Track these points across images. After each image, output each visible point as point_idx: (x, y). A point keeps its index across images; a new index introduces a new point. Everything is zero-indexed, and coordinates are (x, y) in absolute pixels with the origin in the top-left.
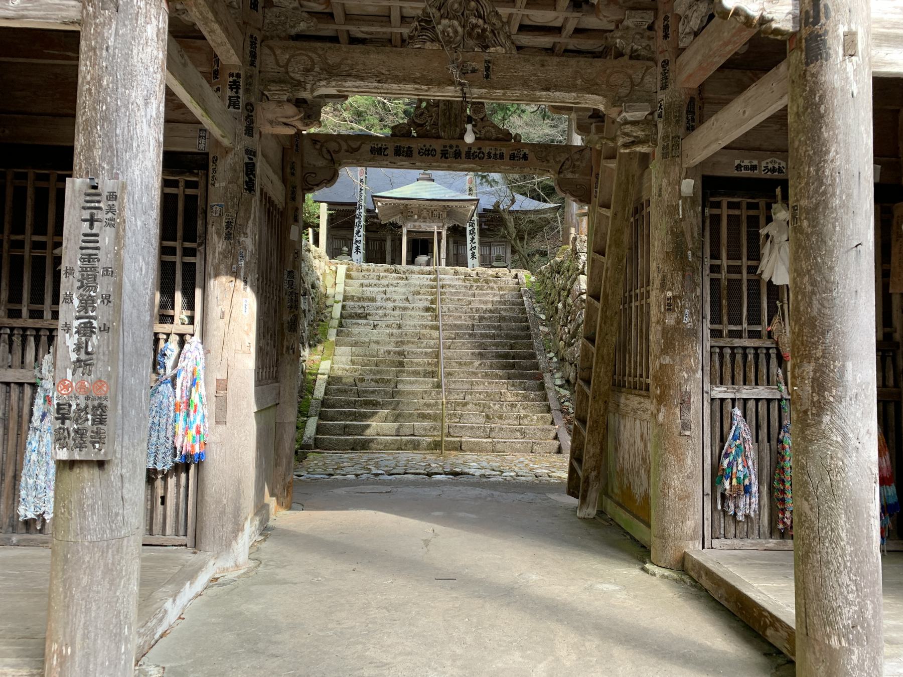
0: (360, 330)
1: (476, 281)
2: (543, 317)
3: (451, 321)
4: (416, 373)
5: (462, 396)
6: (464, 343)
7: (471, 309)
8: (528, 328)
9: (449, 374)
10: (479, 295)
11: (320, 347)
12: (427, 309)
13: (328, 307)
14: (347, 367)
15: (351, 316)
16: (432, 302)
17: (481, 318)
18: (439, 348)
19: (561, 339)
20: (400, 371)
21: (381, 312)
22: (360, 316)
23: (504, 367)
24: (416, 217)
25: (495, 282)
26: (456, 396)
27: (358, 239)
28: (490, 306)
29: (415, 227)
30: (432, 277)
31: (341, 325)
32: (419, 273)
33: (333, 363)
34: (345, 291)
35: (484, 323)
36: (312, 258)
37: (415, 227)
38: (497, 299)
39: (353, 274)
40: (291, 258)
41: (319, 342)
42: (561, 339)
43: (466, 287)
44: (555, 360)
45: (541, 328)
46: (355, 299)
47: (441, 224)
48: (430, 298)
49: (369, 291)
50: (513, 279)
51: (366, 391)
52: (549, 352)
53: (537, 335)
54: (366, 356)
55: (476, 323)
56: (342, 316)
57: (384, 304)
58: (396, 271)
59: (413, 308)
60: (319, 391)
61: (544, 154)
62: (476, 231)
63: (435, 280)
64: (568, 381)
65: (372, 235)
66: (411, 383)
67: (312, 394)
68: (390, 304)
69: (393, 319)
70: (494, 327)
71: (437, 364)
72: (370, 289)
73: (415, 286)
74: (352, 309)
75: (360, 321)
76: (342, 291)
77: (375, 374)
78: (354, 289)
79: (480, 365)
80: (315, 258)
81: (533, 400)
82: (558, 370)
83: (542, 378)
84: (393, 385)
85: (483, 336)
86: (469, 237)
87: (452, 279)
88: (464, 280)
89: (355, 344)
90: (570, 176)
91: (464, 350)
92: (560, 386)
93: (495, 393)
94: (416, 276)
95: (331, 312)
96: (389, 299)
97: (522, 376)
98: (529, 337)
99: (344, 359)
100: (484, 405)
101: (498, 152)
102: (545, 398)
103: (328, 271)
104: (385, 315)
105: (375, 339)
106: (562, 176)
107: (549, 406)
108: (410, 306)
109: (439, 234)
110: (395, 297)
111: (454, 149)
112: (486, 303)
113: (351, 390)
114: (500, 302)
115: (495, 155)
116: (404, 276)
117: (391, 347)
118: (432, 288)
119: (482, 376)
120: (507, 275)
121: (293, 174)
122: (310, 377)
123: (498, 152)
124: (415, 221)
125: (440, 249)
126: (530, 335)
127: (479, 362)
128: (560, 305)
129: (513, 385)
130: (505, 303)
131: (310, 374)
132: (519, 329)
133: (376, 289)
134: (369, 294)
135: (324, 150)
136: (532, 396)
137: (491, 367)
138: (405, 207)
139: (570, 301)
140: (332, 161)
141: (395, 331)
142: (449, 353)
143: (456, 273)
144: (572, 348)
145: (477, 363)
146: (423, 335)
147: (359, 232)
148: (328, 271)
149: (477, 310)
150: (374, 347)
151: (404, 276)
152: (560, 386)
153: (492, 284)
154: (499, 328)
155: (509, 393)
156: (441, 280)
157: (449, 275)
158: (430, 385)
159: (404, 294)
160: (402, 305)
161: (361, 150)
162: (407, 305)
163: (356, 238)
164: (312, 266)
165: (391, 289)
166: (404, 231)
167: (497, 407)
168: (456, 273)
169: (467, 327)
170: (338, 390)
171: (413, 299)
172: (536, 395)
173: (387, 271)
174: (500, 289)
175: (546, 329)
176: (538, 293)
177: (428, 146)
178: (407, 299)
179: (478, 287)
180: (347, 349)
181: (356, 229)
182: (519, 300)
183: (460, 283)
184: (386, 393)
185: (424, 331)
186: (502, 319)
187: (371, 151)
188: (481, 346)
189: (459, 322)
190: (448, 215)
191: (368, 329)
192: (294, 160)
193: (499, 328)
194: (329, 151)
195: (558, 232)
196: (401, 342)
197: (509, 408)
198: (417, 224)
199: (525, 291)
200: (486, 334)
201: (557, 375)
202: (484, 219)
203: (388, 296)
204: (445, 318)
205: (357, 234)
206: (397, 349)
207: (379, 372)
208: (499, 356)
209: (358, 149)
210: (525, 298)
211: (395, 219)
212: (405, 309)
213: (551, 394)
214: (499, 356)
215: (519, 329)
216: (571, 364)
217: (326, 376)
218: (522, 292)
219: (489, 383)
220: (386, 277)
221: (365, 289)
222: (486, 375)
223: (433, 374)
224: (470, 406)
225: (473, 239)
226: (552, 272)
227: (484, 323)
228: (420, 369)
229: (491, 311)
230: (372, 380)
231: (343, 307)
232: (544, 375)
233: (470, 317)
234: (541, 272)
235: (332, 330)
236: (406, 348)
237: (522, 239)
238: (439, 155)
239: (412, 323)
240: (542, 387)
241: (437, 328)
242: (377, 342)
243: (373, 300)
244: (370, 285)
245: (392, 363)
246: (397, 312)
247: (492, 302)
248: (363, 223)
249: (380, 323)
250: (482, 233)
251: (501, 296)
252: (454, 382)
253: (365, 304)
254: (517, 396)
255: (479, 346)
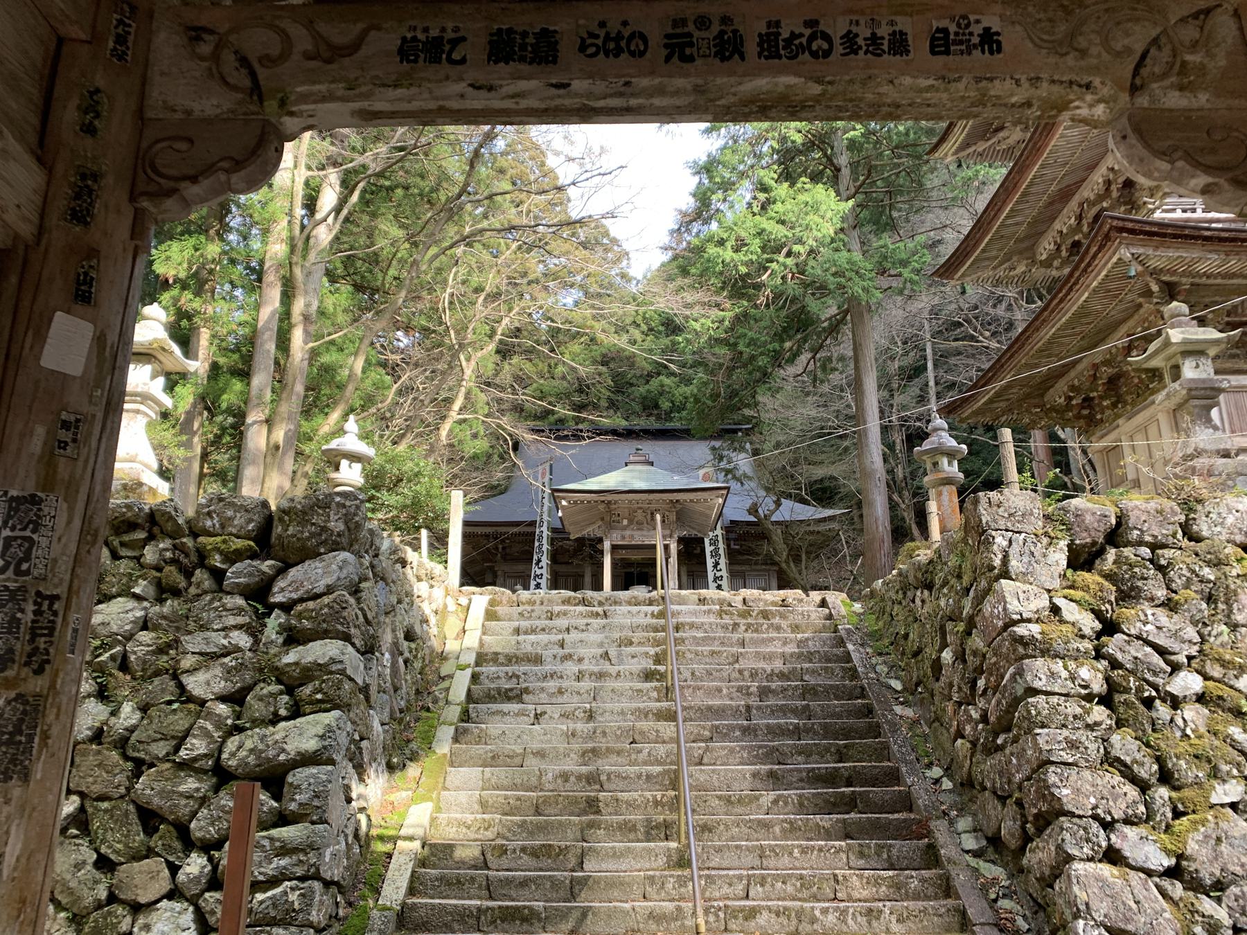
0: (506, 727)
1: (745, 614)
2: (897, 685)
3: (700, 700)
4: (627, 829)
5: (740, 888)
6: (732, 751)
7: (741, 672)
8: (869, 711)
9: (706, 828)
10: (755, 642)
11: (413, 770)
12: (648, 676)
13: (443, 679)
14: (469, 818)
15: (490, 697)
16: (658, 659)
17: (764, 692)
18: (678, 762)
19: (960, 734)
20: (591, 825)
21: (552, 685)
22: (508, 696)
23: (832, 806)
24: (625, 522)
25: (783, 616)
26: (726, 890)
27: (539, 572)
28: (778, 665)
29: (623, 538)
30: (656, 609)
31: (466, 716)
32: (629, 603)
33: (438, 809)
34: (481, 644)
35: (771, 701)
36: (413, 580)
37: (623, 538)
38: (791, 649)
39: (500, 610)
40: (37, 444)
41: (414, 757)
42: (960, 734)
43: (725, 627)
44: (947, 784)
45: (898, 709)
46: (501, 659)
47: (668, 532)
48: (652, 651)
49: (529, 643)
50: (798, 618)
51: (508, 882)
52: (929, 766)
53: (895, 728)
54: (515, 787)
55: (754, 701)
56: (470, 697)
57: (559, 668)
58: (584, 602)
59: (618, 674)
60: (394, 890)
61: (1062, 28)
62: (721, 552)
63: (662, 615)
64: (995, 841)
65: (562, 569)
66: (616, 855)
67: (377, 892)
68: (571, 668)
69: (576, 698)
70: (795, 712)
71: (675, 805)
72: (532, 637)
73: (622, 628)
74: (492, 680)
75: (506, 707)
76: (476, 644)
77: (531, 834)
78: (501, 641)
79: (775, 802)
80: (419, 579)
81: (916, 897)
82: (962, 811)
83: (929, 834)
84: (573, 862)
85: (774, 732)
86: (710, 562)
87: (695, 613)
88: (720, 613)
89: (493, 760)
90: (1174, 100)
91: (733, 768)
92: (977, 854)
93: (823, 879)
94: (625, 609)
95: (448, 689)
96: (568, 657)
97: (876, 830)
98: (875, 731)
99: (463, 797)
100: (800, 914)
101: (884, 31)
102: (947, 889)
103: (452, 607)
104: (560, 692)
105: (536, 746)
106: (1143, 101)
107: (963, 913)
108: (613, 670)
109: (666, 547)
110: (582, 651)
111: (716, 28)
112: (769, 657)
113: (473, 879)
114: (800, 655)
115: (874, 39)
116: (600, 610)
117: (571, 765)
118: (656, 630)
119: (783, 830)
120: (804, 604)
121: (90, 130)
122: (380, 847)
123: (884, 31)
124: (625, 528)
125: (668, 567)
126: (878, 726)
127: (772, 795)
128: (947, 656)
129: (861, 855)
130: (809, 657)
131: (381, 838)
132: (850, 713)
133: (543, 638)
134: (529, 649)
135: (229, 58)
136: (914, 884)
137: (801, 808)
138: (607, 506)
139: (977, 642)
140: (256, 91)
141: (580, 726)
142: (700, 774)
143: (702, 601)
144: (999, 756)
145: (767, 797)
146: (642, 733)
147: (539, 561)
148: (452, 607)
149: (754, 674)
150: (533, 763)
151: (600, 610)
152: (977, 854)
153: (777, 620)
154: (806, 712)
155: (831, 859)
156: (673, 615)
157: (687, 605)
158: (662, 861)
159: (601, 645)
160: (596, 669)
161: (362, 52)
162: (607, 667)
163: (535, 570)
164: (409, 594)
165: (574, 636)
166: (607, 545)
167: (831, 918)
168: (702, 601)
169: (736, 712)
170: (441, 879)
171: (620, 655)
172: (923, 880)
173: (567, 601)
174: (796, 628)
175: (909, 712)
176: (875, 636)
177: (614, 26)
178: (606, 656)
179: (749, 626)
180: (471, 774)
181: (535, 557)
182: (839, 651)
183: (712, 619)
184: (555, 884)
185: (643, 725)
186: (809, 692)
187: (401, 52)
188: (771, 755)
189: (717, 702)
190: (678, 519)
191: (524, 724)
192: (100, 81)
193: (806, 712)
194: (244, 61)
195: (845, 556)
196: (593, 750)
197: (862, 920)
198: (628, 533)
199: (848, 631)
200: (779, 726)
201: (964, 824)
202: (733, 536)
203: (566, 651)
204: (687, 692)
205: (537, 564)
206: (584, 769)
207: (542, 828)
208: (816, 779)
209: (354, 47)
210: (850, 647)
211: (592, 531)
212: (601, 676)
213: (961, 879)
214: (816, 779)
215: (850, 713)
216: (1003, 800)
217: (416, 845)
218: (843, 633)
219: (804, 851)
220: (565, 614)
221: (521, 638)
222: (792, 830)
223: (667, 830)
224: (763, 919)
225: (716, 565)
226: (905, 589)
227: (771, 701)
228: (636, 817)
229: (782, 676)
230: (523, 849)
231: (475, 678)
232: (933, 824)
233: (739, 689)
234: (873, 594)
235: (444, 728)
236: (606, 765)
237: (797, 559)
238: (657, 50)
239: (617, 706)
240: (931, 857)
241: (671, 716)
242: (541, 754)
243: (537, 660)
244: (533, 631)
245: (573, 805)
246: (586, 684)
247: (783, 655)
248: (546, 547)
249: (548, 708)
250: (731, 554)
251: (800, 643)
252: (719, 850)
253: (520, 669)
254: (877, 884)
255: (767, 755)
